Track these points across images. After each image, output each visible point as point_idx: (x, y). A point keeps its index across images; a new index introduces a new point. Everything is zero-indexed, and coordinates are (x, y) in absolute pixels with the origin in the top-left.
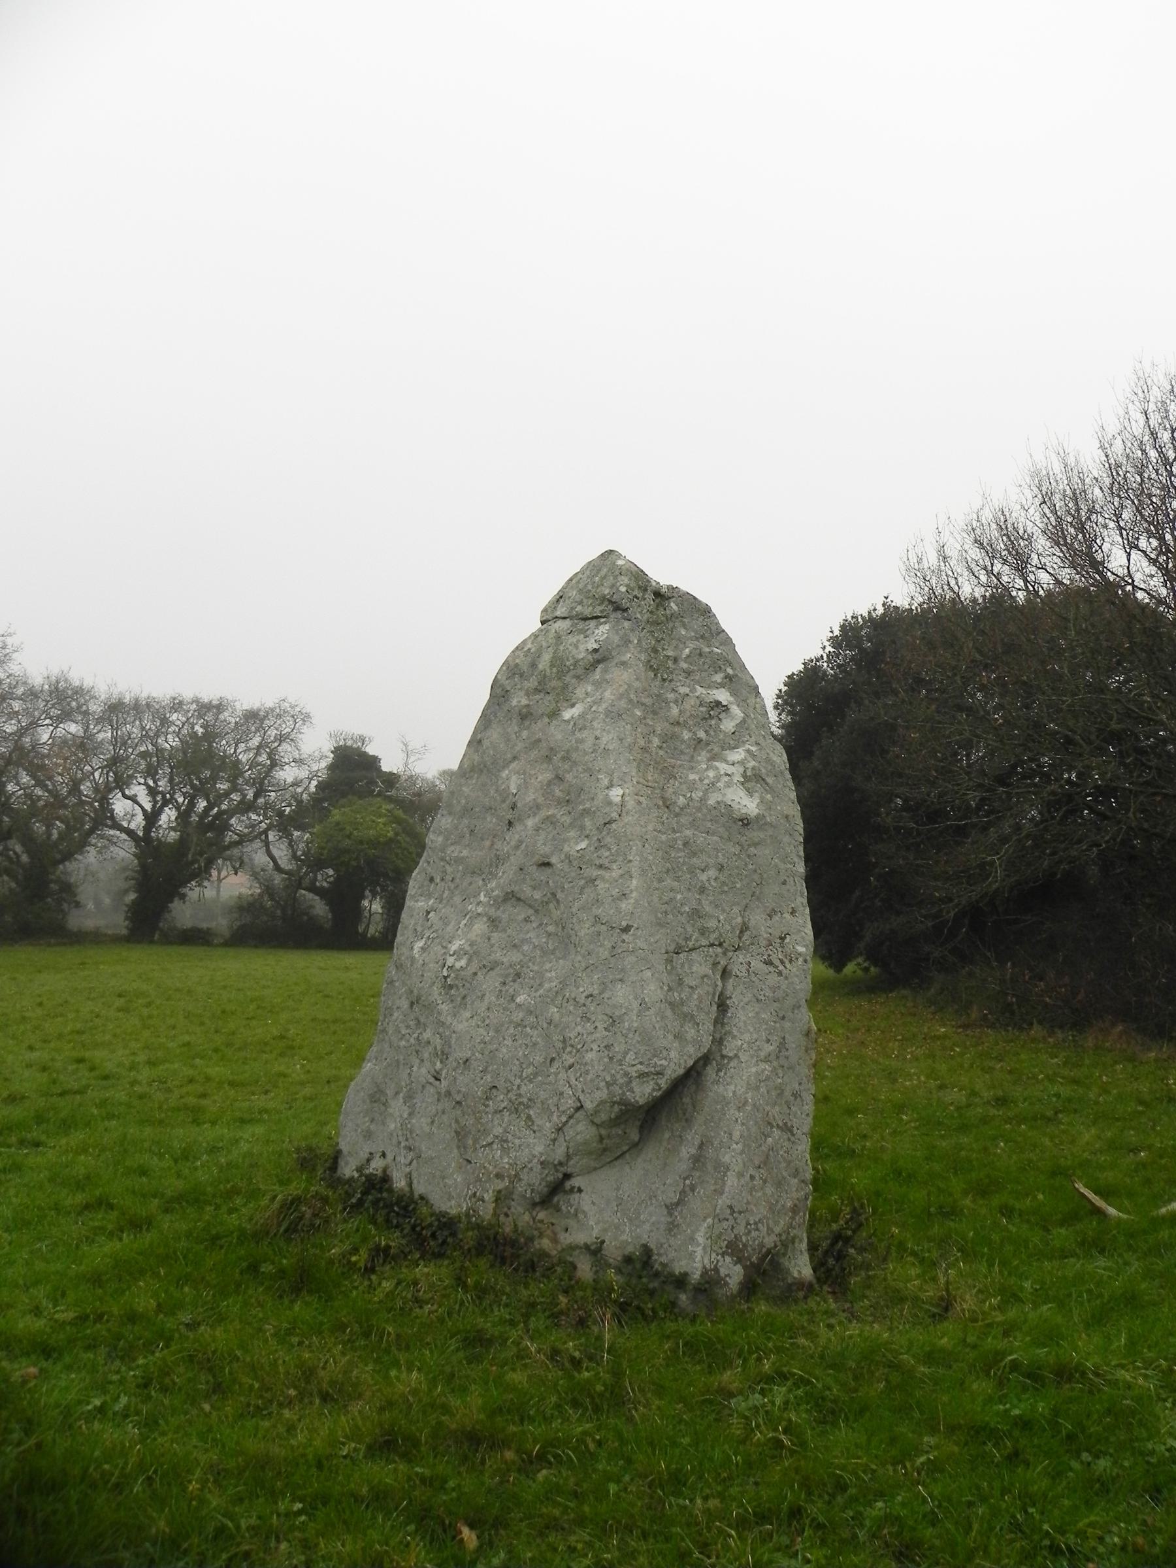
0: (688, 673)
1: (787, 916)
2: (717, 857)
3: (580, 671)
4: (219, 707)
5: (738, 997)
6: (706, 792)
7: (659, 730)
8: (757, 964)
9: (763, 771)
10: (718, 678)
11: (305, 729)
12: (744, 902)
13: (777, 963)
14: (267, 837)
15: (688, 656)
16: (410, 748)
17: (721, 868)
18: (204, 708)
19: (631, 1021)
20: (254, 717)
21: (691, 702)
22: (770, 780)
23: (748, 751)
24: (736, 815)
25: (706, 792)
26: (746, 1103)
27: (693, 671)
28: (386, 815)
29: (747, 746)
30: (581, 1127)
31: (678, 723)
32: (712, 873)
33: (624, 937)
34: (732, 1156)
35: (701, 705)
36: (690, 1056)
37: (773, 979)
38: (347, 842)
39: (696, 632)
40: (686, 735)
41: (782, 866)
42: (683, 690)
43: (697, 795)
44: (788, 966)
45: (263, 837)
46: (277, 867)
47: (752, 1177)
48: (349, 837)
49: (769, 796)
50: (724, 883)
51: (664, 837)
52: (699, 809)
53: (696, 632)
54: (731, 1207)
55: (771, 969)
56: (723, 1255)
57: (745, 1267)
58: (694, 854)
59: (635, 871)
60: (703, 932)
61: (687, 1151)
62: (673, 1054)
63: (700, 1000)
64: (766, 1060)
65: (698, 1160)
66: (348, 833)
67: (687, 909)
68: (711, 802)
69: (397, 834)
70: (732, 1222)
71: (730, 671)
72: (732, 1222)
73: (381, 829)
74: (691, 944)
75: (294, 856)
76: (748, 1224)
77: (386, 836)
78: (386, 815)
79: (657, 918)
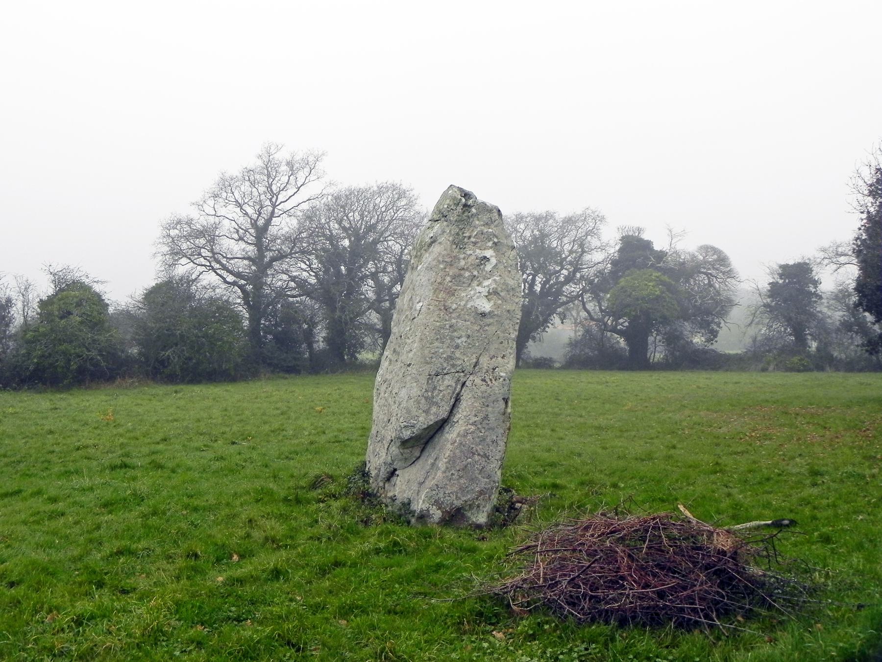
0: (475, 243)
1: (499, 359)
2: (467, 332)
3: (426, 247)
4: (548, 216)
5: (466, 395)
6: (467, 301)
7: (451, 273)
8: (478, 381)
9: (499, 289)
10: (490, 244)
11: (601, 227)
12: (480, 352)
13: (488, 380)
14: (583, 298)
15: (476, 235)
16: (673, 233)
17: (468, 337)
18: (538, 219)
19: (404, 404)
20: (569, 221)
21: (473, 257)
22: (502, 294)
23: (495, 280)
24: (479, 312)
25: (467, 301)
26: (455, 441)
27: (478, 242)
28: (655, 280)
29: (495, 278)
30: (394, 448)
31: (463, 269)
32: (464, 339)
33: (408, 368)
34: (442, 464)
35: (477, 259)
36: (431, 420)
37: (484, 388)
38: (628, 300)
39: (484, 221)
40: (467, 274)
41: (501, 335)
42: (469, 252)
43: (463, 303)
44: (494, 382)
45: (580, 299)
46: (592, 319)
47: (452, 474)
48: (629, 296)
49: (500, 302)
50: (469, 344)
51: (438, 324)
52: (462, 310)
53: (484, 221)
54: (437, 485)
55: (484, 383)
56: (432, 505)
57: (443, 512)
58: (455, 331)
59: (417, 339)
60: (453, 366)
61: (430, 461)
62: (421, 419)
63: (444, 396)
64: (474, 424)
65: (433, 465)
66: (629, 293)
67: (445, 356)
68: (469, 306)
69: (663, 292)
70: (437, 491)
71: (496, 240)
72: (437, 491)
73: (651, 290)
74: (445, 371)
75: (601, 311)
76: (445, 493)
77: (654, 294)
78: (655, 280)
79: (425, 359)
